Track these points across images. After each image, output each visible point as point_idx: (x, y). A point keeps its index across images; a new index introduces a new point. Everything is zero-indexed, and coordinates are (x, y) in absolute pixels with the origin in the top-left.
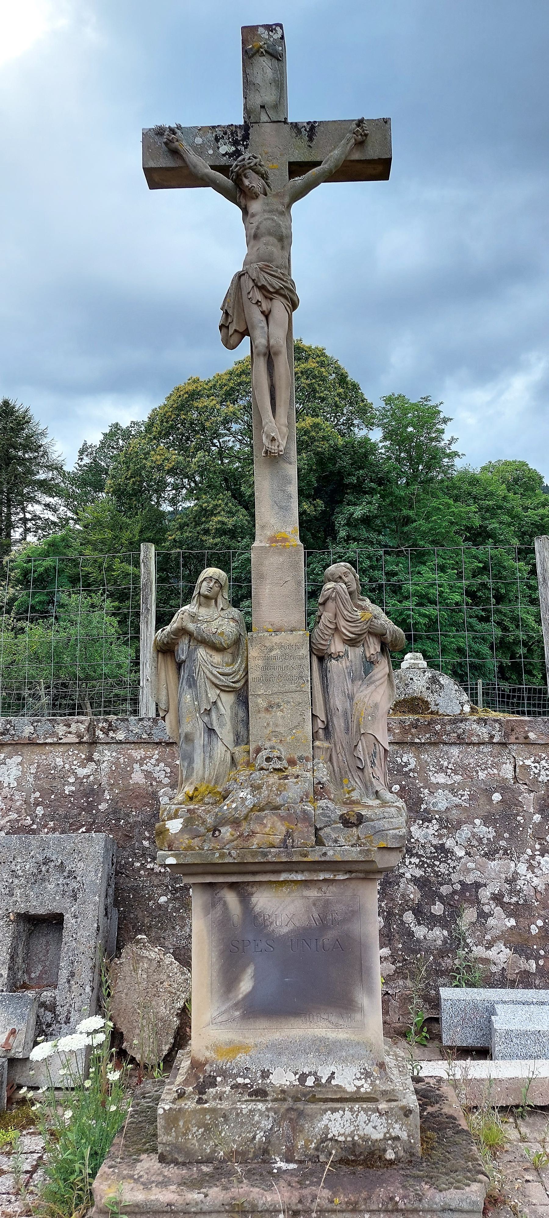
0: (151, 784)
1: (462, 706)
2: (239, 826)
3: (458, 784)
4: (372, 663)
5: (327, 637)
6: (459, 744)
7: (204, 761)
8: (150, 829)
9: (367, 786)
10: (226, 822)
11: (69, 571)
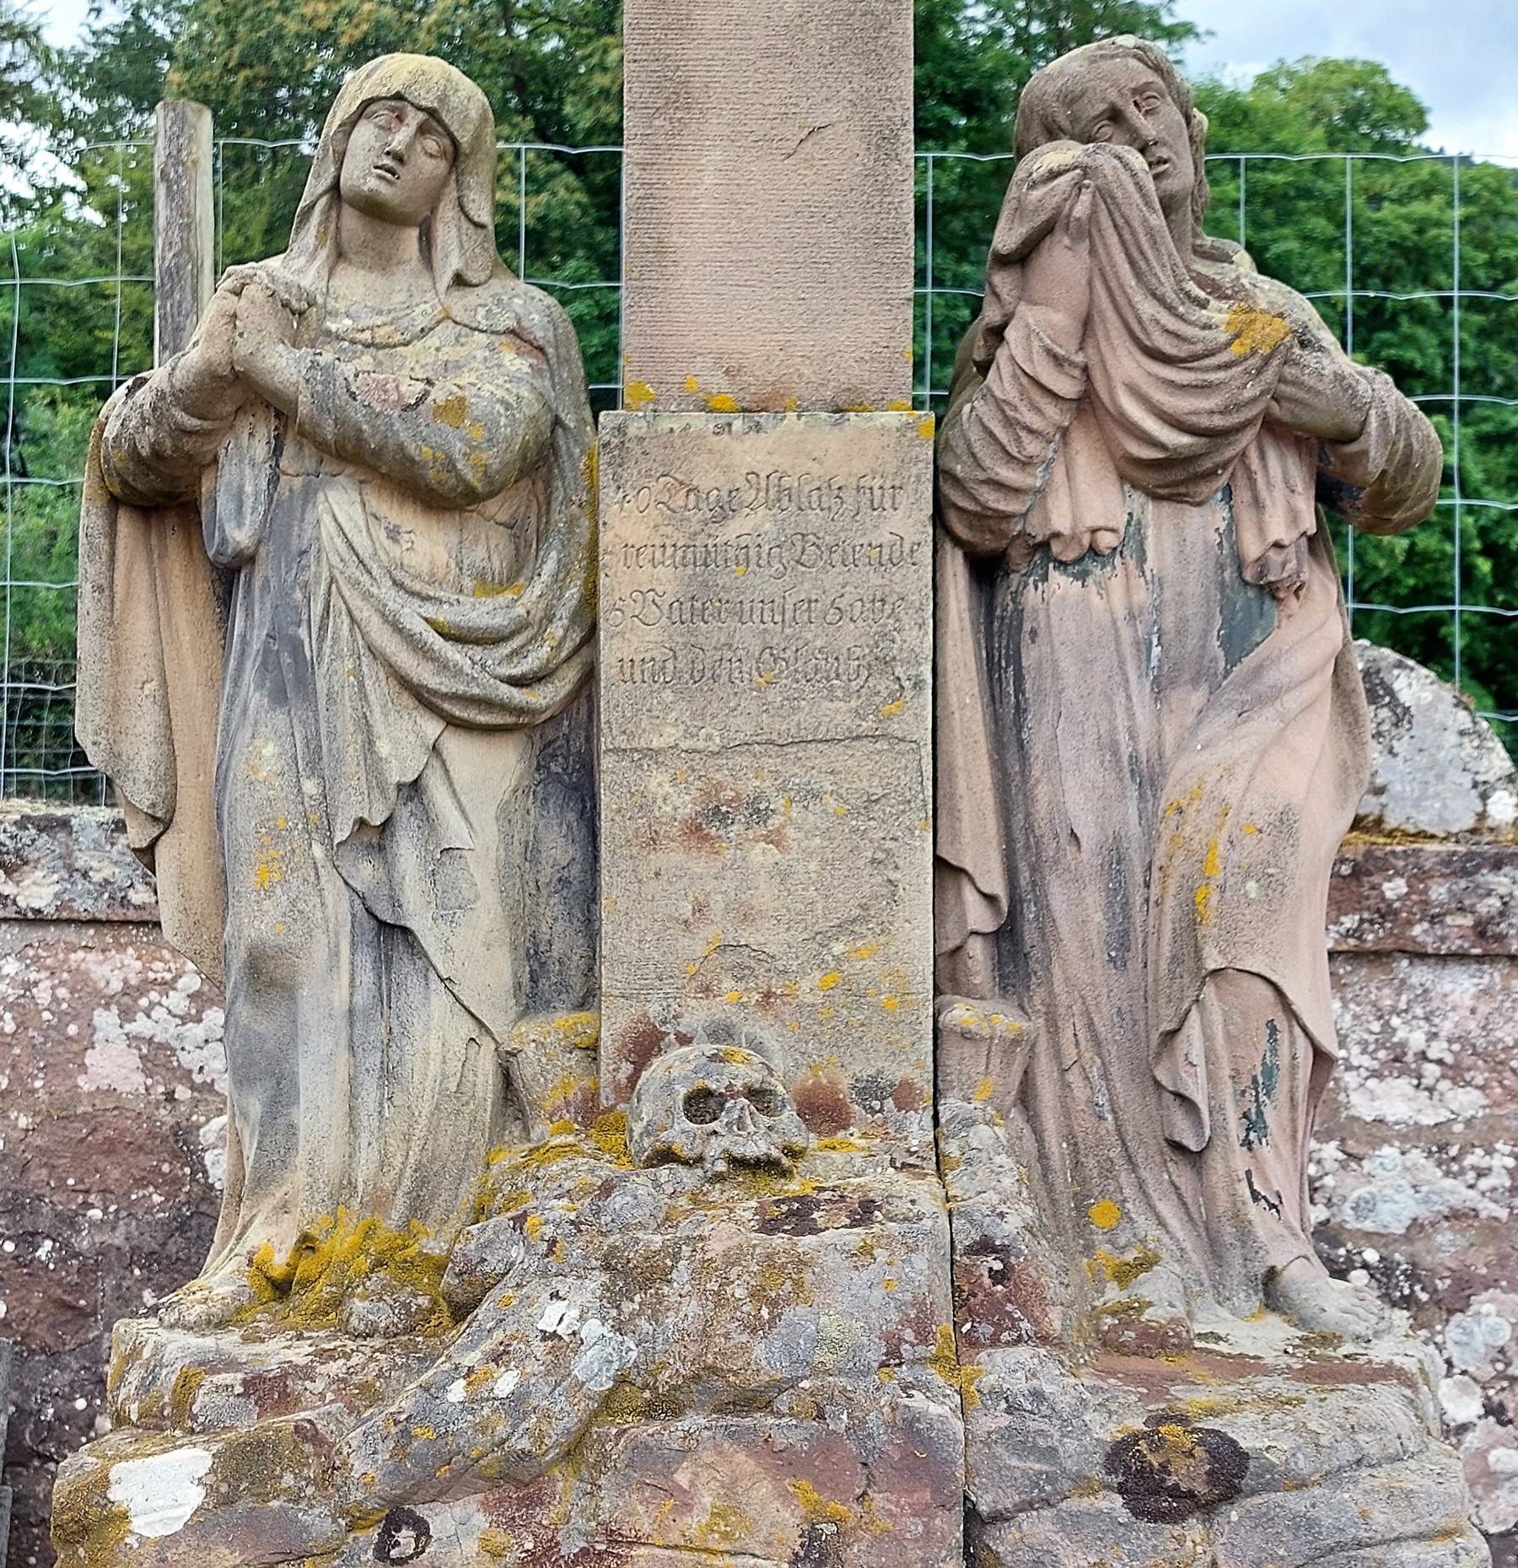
0: (170, 1097)
1: (1484, 797)
2: (533, 1501)
3: (1469, 1123)
4: (1270, 591)
5: (1032, 447)
6: (1479, 959)
7: (353, 1096)
8: (162, 1279)
9: (1217, 1240)
10: (457, 1476)
11: (63, 339)
